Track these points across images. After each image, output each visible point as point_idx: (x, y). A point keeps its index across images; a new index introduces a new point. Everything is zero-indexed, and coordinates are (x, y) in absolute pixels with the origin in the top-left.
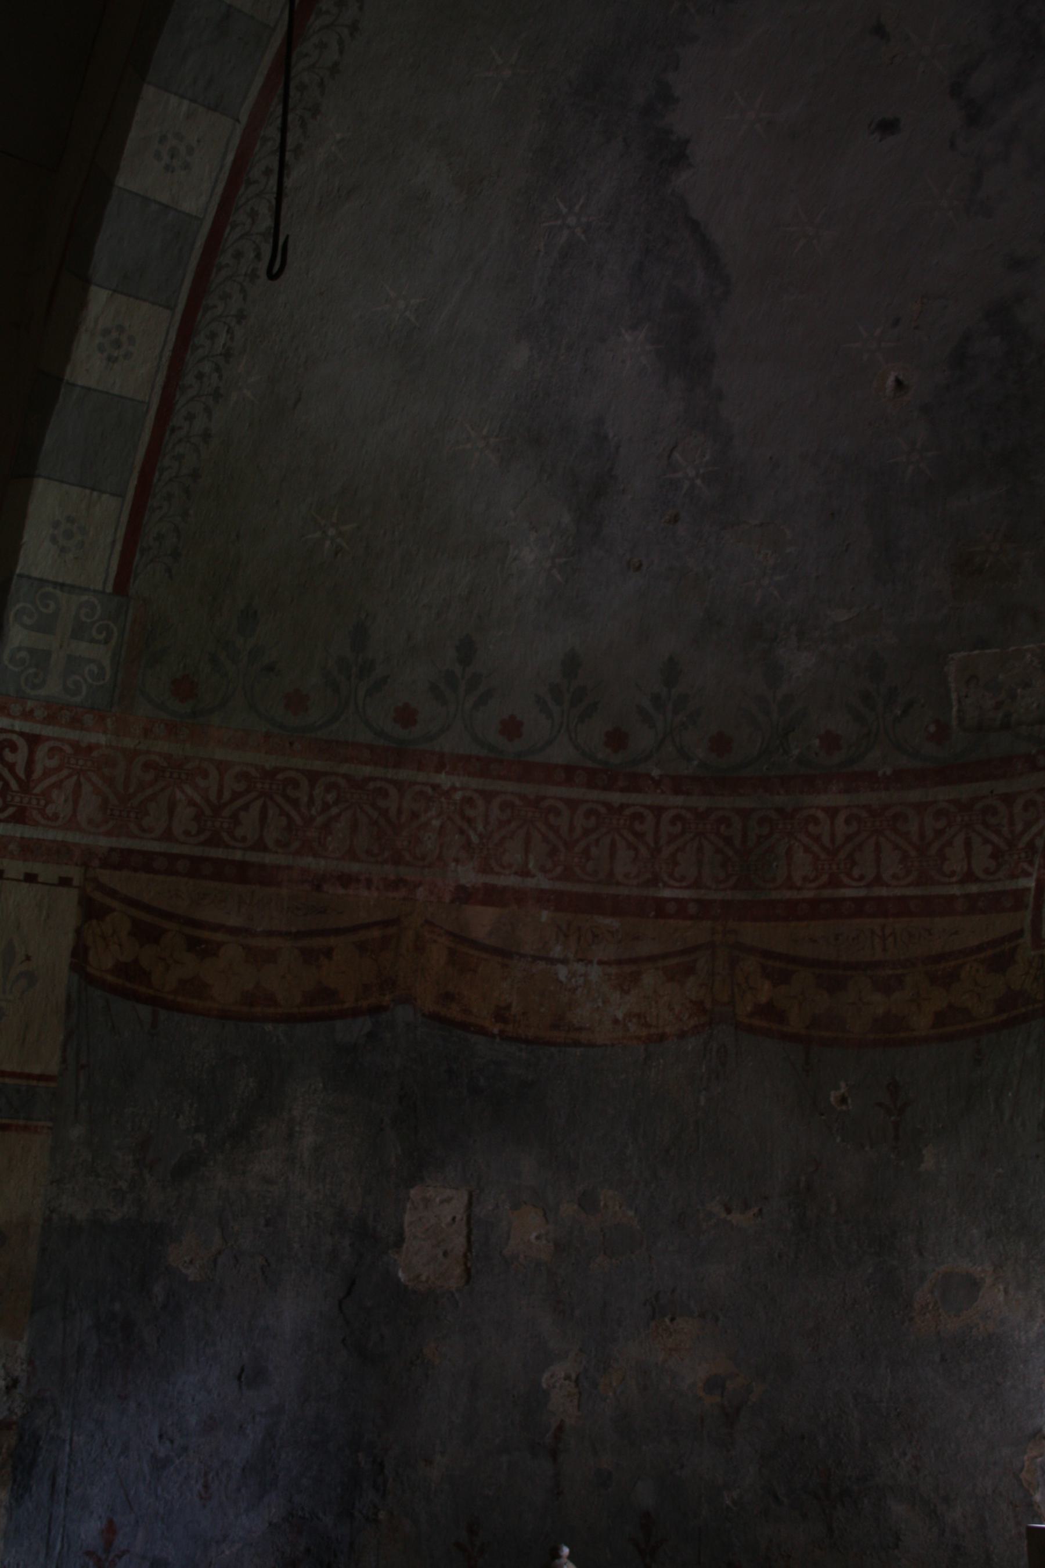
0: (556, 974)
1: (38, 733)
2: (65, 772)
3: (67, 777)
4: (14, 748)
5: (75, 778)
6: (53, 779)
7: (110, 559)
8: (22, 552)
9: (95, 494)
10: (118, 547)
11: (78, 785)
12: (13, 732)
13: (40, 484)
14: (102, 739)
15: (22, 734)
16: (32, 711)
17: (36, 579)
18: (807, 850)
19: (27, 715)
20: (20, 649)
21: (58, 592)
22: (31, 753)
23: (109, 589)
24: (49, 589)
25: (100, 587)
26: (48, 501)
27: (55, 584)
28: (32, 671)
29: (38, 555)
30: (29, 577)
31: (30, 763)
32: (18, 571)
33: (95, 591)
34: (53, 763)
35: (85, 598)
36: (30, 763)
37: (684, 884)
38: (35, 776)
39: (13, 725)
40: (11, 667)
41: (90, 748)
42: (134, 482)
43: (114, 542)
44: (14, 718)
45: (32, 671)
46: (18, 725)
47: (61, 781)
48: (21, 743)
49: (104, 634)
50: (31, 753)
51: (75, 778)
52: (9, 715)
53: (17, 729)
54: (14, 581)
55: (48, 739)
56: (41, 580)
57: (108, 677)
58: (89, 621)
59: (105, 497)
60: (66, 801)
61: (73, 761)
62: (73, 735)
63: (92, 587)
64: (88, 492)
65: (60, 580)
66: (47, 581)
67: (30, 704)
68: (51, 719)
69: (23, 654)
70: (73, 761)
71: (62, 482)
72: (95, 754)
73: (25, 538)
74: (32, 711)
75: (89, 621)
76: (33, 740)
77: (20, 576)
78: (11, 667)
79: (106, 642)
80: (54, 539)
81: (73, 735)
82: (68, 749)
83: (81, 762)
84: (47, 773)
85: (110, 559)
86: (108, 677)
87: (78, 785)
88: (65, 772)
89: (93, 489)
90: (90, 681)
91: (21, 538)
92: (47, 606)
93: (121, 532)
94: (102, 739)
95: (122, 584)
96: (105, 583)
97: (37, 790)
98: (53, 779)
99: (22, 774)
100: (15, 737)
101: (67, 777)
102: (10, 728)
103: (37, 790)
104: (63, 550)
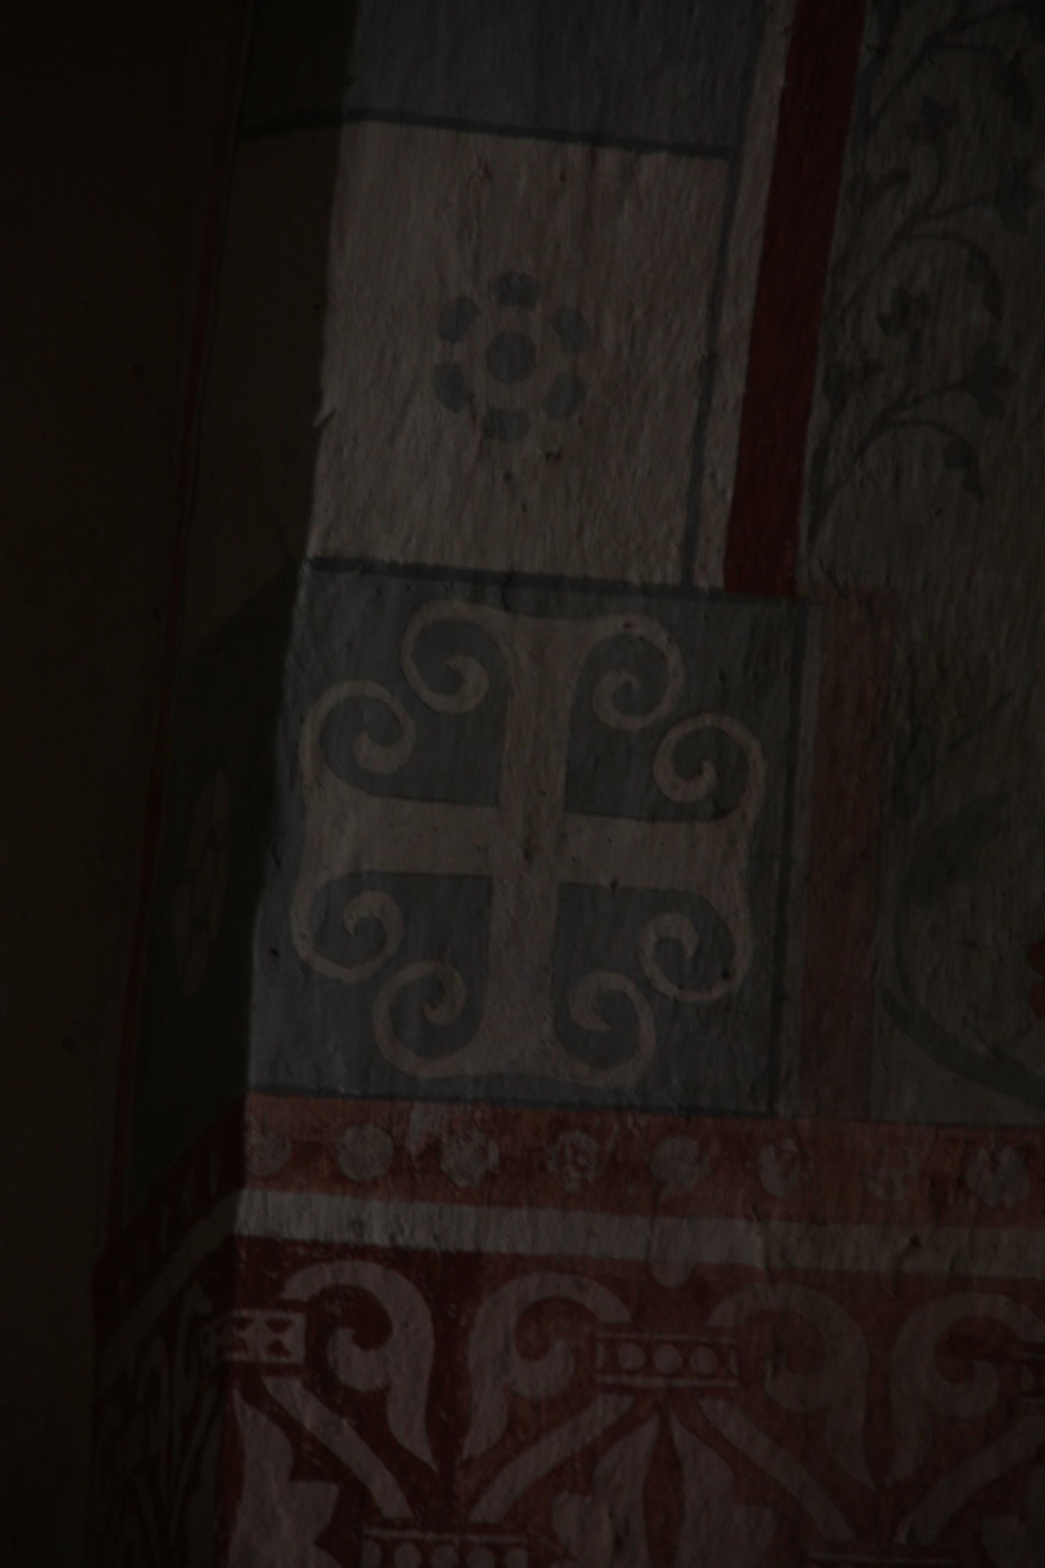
0: (670, 640)
1: (468, 1247)
2: (603, 1412)
3: (616, 1433)
4: (372, 1326)
5: (648, 1433)
6: (550, 1451)
7: (698, 439)
8: (322, 463)
9: (609, 158)
10: (732, 382)
11: (667, 1464)
12: (363, 1252)
13: (370, 152)
14: (749, 1244)
15: (400, 1259)
16: (433, 1150)
17: (392, 569)
18: (313, 1462)
19: (416, 1172)
20: (356, 882)
21: (493, 617)
22: (450, 1337)
23: (711, 575)
24: (457, 607)
25: (670, 573)
26: (412, 219)
27: (477, 582)
28: (413, 973)
29: (393, 464)
30: (365, 566)
31: (447, 1387)
32: (313, 548)
33: (646, 590)
34: (545, 1376)
35: (607, 627)
36: (447, 1387)
37: (530, 1286)
38: (475, 1443)
39: (358, 1224)
40: (324, 967)
41: (701, 1289)
42: (770, 85)
43: (710, 363)
44: (360, 1189)
45: (413, 973)
46: (381, 1221)
47: (592, 1455)
48: (402, 1300)
49: (709, 773)
50: (450, 1337)
51: (648, 1433)
52: (337, 1181)
53: (378, 1237)
54: (302, 596)
55: (515, 1266)
56: (416, 572)
57: (742, 964)
58: (635, 724)
59: (649, 165)
60: (619, 1544)
61: (631, 1357)
62: (620, 1238)
63: (633, 577)
64: (576, 153)
65: (499, 564)
66: (439, 573)
67: (421, 1122)
68: (518, 1179)
69: (371, 903)
70: (631, 1357)
71: (460, 125)
72: (723, 1314)
73: (332, 399)
74: (433, 1150)
75: (635, 724)
76: (452, 1281)
77: (326, 564)
78: (324, 967)
79: (720, 809)
80: (453, 387)
81: (620, 1238)
82: (606, 1306)
83: (667, 1358)
84: (521, 1428)
85: (698, 439)
86: (742, 964)
87: (667, 1464)
88: (603, 1412)
89: (595, 140)
90: (665, 986)
91: (316, 398)
92: (454, 682)
93: (738, 313)
94: (749, 1244)
95: (761, 547)
96: (688, 548)
97: (490, 1507)
98: (550, 1451)
99: (410, 1431)
100: (370, 1276)
101: (616, 1433)
102: (349, 1237)
103: (490, 1507)
104: (495, 428)
